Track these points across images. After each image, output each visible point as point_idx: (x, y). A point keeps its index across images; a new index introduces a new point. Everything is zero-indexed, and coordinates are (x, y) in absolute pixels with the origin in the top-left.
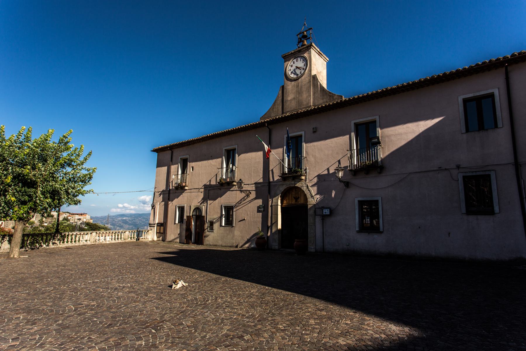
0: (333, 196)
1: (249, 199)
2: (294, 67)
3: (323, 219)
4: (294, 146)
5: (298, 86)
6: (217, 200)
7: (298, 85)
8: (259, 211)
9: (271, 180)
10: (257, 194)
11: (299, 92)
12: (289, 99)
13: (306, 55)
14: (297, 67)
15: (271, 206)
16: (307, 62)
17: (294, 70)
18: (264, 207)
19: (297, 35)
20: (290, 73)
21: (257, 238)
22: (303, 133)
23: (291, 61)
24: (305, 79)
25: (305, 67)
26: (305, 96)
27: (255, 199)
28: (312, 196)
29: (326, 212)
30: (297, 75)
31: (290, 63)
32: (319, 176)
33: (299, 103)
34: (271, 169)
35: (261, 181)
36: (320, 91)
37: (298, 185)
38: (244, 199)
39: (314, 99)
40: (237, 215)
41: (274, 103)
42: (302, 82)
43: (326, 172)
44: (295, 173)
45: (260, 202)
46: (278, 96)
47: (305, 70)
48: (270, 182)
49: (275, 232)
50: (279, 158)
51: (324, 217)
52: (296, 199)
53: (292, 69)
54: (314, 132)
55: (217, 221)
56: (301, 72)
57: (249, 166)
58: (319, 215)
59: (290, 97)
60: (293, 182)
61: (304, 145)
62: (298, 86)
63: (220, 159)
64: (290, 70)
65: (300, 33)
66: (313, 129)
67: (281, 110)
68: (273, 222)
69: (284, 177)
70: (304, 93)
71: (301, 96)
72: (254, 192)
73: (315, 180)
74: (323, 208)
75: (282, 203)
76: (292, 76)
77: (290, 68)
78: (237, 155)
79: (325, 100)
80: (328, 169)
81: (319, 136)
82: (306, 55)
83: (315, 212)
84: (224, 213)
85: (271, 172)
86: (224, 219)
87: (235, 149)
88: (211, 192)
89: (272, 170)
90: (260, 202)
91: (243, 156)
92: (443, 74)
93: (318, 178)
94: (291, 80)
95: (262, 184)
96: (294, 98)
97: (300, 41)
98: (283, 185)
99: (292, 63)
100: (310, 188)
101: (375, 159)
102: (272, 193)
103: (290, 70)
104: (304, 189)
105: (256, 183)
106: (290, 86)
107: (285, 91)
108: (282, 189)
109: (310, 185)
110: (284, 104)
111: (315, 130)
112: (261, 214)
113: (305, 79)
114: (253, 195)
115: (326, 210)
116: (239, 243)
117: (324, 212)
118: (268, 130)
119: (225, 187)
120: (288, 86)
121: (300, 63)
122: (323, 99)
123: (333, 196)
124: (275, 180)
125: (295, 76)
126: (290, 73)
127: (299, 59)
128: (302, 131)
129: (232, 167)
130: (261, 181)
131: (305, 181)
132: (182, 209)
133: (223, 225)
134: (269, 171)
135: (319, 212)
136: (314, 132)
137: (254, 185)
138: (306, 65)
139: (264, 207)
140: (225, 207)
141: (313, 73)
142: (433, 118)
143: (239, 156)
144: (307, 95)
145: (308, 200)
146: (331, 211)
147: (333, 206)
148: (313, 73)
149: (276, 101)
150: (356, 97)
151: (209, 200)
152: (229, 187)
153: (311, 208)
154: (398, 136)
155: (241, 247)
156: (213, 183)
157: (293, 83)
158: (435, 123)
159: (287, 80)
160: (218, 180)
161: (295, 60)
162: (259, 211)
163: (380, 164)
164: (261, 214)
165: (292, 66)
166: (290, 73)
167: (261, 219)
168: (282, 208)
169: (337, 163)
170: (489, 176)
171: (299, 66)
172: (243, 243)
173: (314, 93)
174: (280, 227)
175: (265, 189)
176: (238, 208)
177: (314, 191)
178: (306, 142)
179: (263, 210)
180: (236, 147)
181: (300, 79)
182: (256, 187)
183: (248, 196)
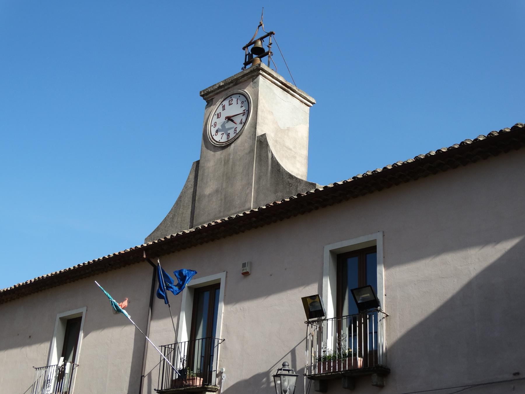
2: (223, 119)
4: (355, 273)
5: (226, 162)
7: (228, 161)
11: (228, 177)
13: (248, 90)
16: (249, 106)
17: (223, 125)
19: (244, 49)
20: (213, 133)
22: (221, 276)
23: (218, 103)
24: (242, 145)
26: (238, 185)
33: (227, 202)
36: (272, 172)
39: (257, 192)
46: (186, 187)
47: (245, 123)
59: (208, 188)
61: (222, 308)
63: (47, 345)
66: (244, 265)
67: (188, 219)
77: (215, 119)
78: (81, 335)
79: (280, 194)
81: (254, 285)
82: (248, 90)
85: (146, 381)
89: (150, 374)
91: (94, 336)
92: (460, 145)
96: (217, 191)
97: (249, 60)
99: (220, 109)
101: (324, 368)
107: (200, 173)
110: (197, 204)
111: (247, 269)
113: (242, 145)
118: (152, 269)
121: (234, 108)
122: (276, 192)
125: (224, 139)
127: (235, 100)
129: (65, 365)
132: (155, 390)
134: (142, 377)
138: (247, 113)
141: (259, 132)
142: (497, 240)
143: (85, 336)
148: (259, 132)
149: (180, 197)
150: (234, 216)
154: (412, 290)
157: (219, 154)
158: (503, 252)
159: (207, 147)
161: (226, 103)
163: (381, 362)
166: (213, 133)
173: (259, 179)
181: (233, 146)
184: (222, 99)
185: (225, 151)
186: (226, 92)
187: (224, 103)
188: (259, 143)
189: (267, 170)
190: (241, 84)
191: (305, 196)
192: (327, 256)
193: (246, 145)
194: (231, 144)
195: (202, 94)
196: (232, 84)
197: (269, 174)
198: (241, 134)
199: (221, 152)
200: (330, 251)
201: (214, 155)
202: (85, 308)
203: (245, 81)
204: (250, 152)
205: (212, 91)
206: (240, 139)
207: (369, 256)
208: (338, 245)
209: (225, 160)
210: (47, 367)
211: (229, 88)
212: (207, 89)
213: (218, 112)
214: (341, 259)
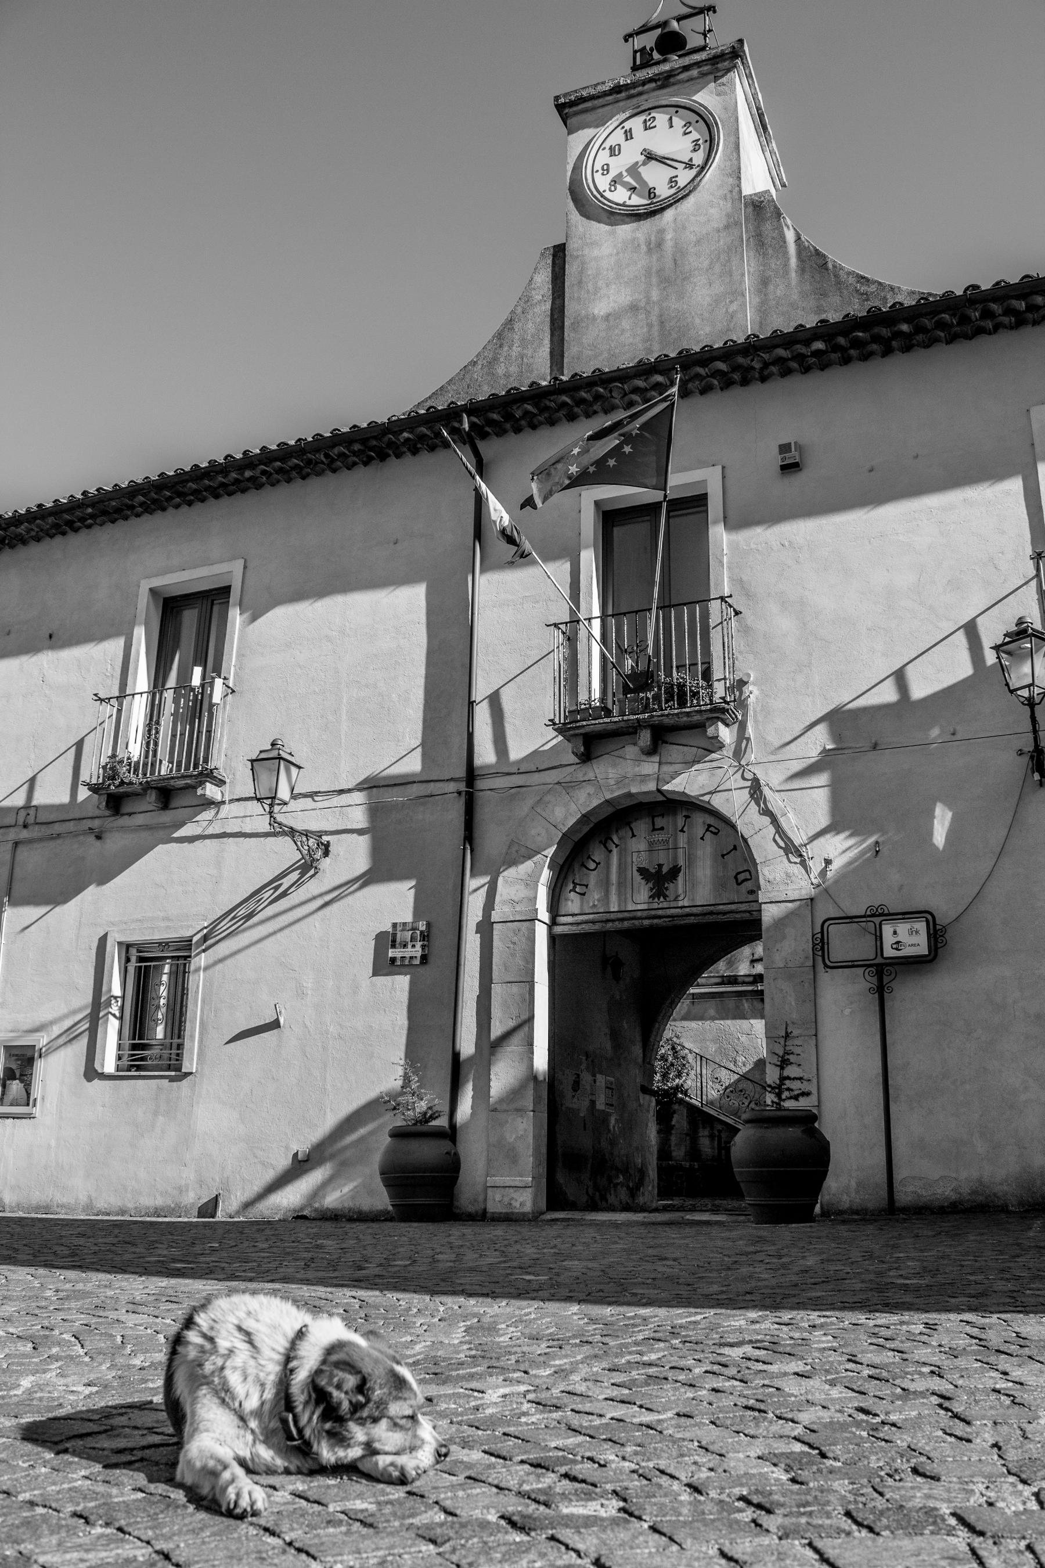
0: (939, 838)
1: (313, 887)
2: (631, 154)
3: (881, 991)
4: (653, 554)
5: (656, 246)
6: (72, 906)
7: (660, 245)
8: (385, 965)
9: (485, 754)
10: (376, 852)
12: (600, 308)
14: (650, 157)
15: (485, 928)
18: (425, 937)
21: (398, 1134)
25: (698, 158)
27: (368, 879)
28: (790, 849)
29: (908, 938)
30: (651, 193)
31: (610, 133)
32: (837, 720)
34: (481, 690)
35: (413, 765)
36: (802, 270)
37: (690, 782)
38: (274, 888)
40: (218, 993)
41: (499, 335)
42: (680, 227)
43: (888, 694)
44: (658, 701)
45: (395, 903)
46: (526, 300)
48: (472, 774)
49: (514, 1094)
50: (536, 628)
51: (885, 974)
52: (660, 879)
53: (619, 165)
54: (790, 468)
55: (70, 1037)
56: (673, 181)
57: (329, 675)
58: (852, 965)
60: (650, 767)
62: (656, 246)
63: (115, 647)
64: (606, 169)
65: (645, 29)
66: (784, 448)
68: (497, 1030)
69: (588, 737)
70: (700, 280)
71: (681, 296)
72: (363, 842)
73: (820, 740)
74: (879, 915)
75: (554, 908)
76: (620, 195)
77: (604, 157)
80: (900, 677)
81: (798, 483)
83: (821, 944)
84: (117, 990)
85: (482, 715)
86: (113, 1024)
87: (226, 590)
88: (32, 859)
90: (395, 903)
91: (281, 618)
93: (836, 735)
94: (614, 216)
95: (415, 790)
96: (634, 308)
98: (569, 786)
99: (618, 137)
100: (775, 801)
102: (493, 836)
103: (606, 169)
104: (733, 803)
105: (371, 785)
106: (600, 247)
108: (567, 812)
109: (772, 777)
111: (793, 456)
112: (402, 983)
114: (352, 856)
115: (903, 928)
116: (226, 1185)
117: (888, 938)
119: (139, 820)
120: (594, 244)
123: (939, 838)
124: (517, 752)
126: (603, 183)
128: (702, 464)
130: (413, 765)
131: (738, 754)
133: (109, 1066)
134: (471, 704)
135: (845, 944)
136: (790, 468)
137: (359, 797)
139: (425, 937)
140: (126, 947)
144: (718, 288)
145: (765, 873)
146: (937, 936)
147: (945, 909)
151: (15, 903)
152: (167, 817)
153: (781, 923)
155: (247, 1205)
156: (54, 792)
157: (625, 230)
160: (91, 771)
161: (636, 124)
162: (385, 965)
164: (402, 983)
165: (614, 151)
167: (402, 1020)
168: (553, 940)
169: (961, 638)
170: (663, 1194)
171: (660, 149)
172: (257, 1187)
174: (541, 1061)
175: (439, 816)
176: (223, 949)
177: (807, 809)
178: (734, 523)
179: (423, 956)
180: (232, 571)
182: (374, 811)
183: (307, 867)
184: (628, 114)
185: (646, 225)
186: (635, 101)
187: (627, 125)
188: (750, 209)
189: (786, 265)
190: (676, 87)
191: (256, 455)
192: (143, 599)
193: (714, 212)
194: (663, 209)
195: (562, 100)
196: (653, 85)
197: (793, 275)
198: (695, 188)
199: (635, 225)
200: (151, 590)
201: (613, 233)
202: (240, 563)
203: (691, 79)
204: (727, 227)
205: (592, 98)
206: (691, 199)
207: (685, 521)
208: (157, 582)
209: (648, 243)
210: (120, 698)
211: (640, 94)
212: (576, 91)
213: (612, 141)
214: (171, 607)
